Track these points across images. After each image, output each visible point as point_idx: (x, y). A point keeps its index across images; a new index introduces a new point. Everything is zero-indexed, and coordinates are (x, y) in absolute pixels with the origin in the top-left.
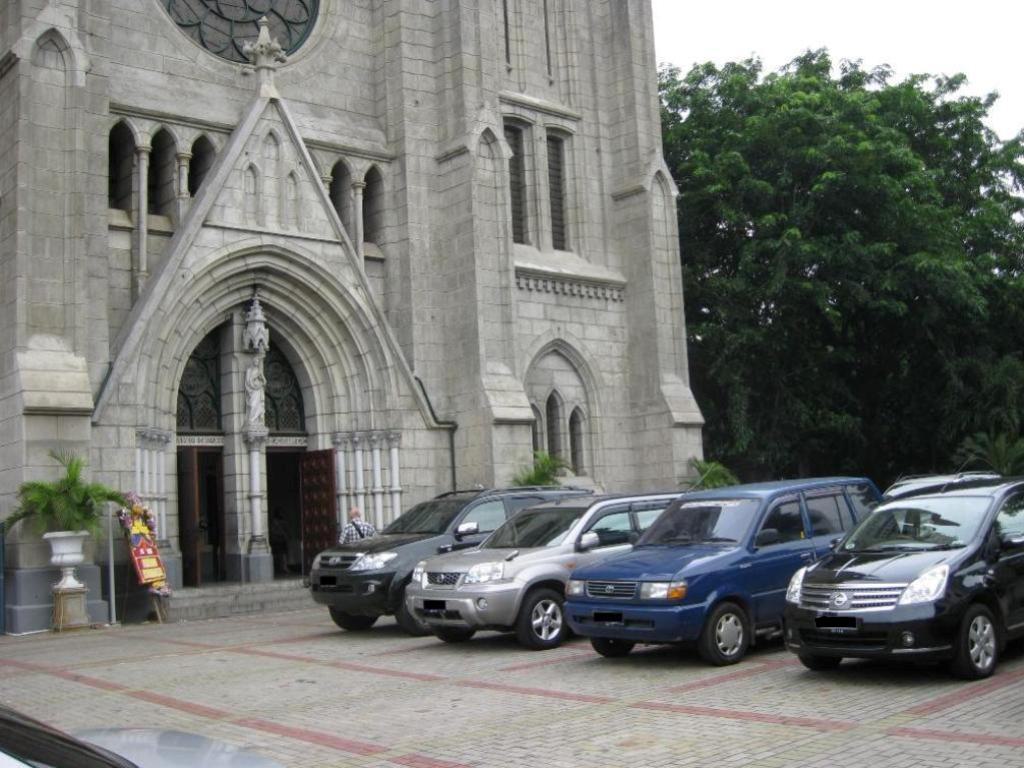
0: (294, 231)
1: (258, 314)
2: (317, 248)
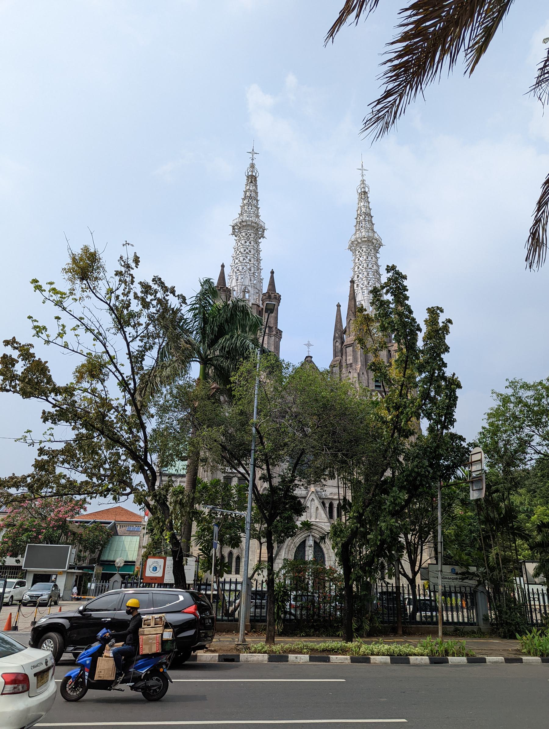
0: (318, 520)
1: (311, 538)
2: (323, 524)
